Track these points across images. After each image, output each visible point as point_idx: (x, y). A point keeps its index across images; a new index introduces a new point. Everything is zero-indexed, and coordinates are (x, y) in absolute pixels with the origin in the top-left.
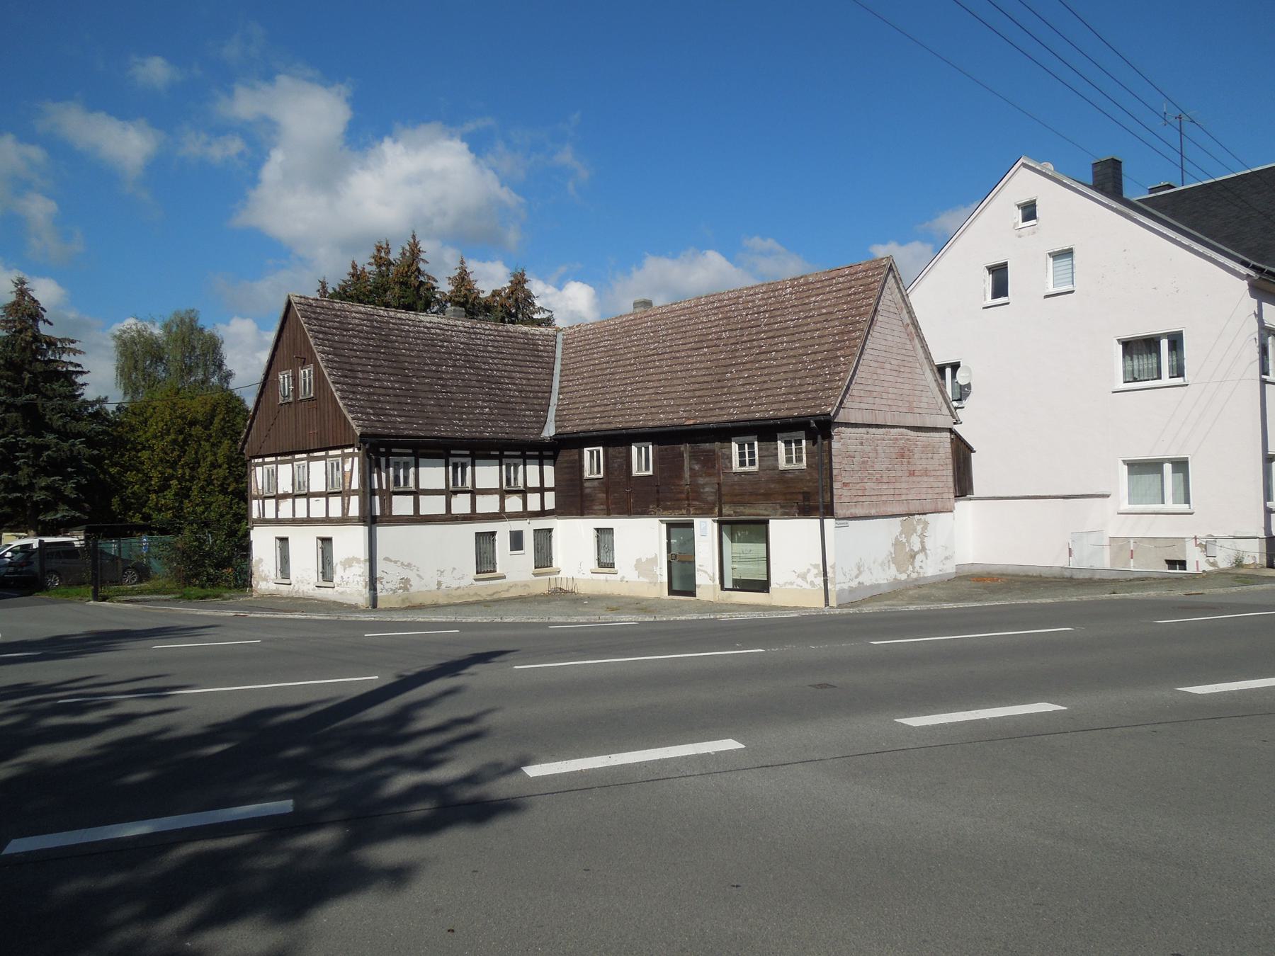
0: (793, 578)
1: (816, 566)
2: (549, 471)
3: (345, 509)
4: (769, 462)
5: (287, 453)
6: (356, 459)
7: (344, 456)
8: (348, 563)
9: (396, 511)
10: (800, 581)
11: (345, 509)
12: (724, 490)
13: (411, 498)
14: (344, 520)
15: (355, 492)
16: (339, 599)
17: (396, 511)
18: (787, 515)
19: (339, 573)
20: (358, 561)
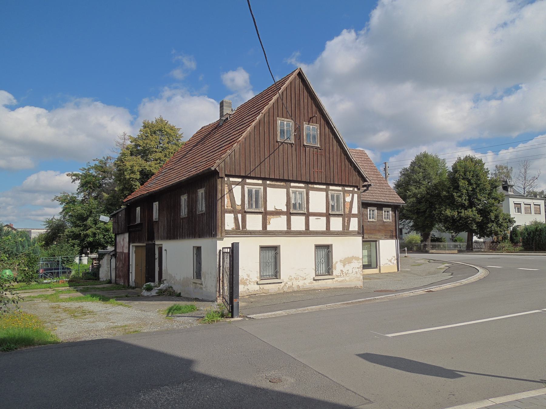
0: (387, 262)
1: (394, 257)
2: (482, 218)
3: (346, 226)
4: (380, 218)
5: (284, 181)
6: (356, 196)
7: (345, 192)
8: (347, 261)
9: (249, 227)
10: (389, 263)
11: (346, 226)
12: (365, 228)
13: (303, 218)
14: (345, 232)
15: (354, 216)
16: (338, 285)
17: (249, 227)
18: (386, 238)
19: (338, 268)
20: (357, 259)
